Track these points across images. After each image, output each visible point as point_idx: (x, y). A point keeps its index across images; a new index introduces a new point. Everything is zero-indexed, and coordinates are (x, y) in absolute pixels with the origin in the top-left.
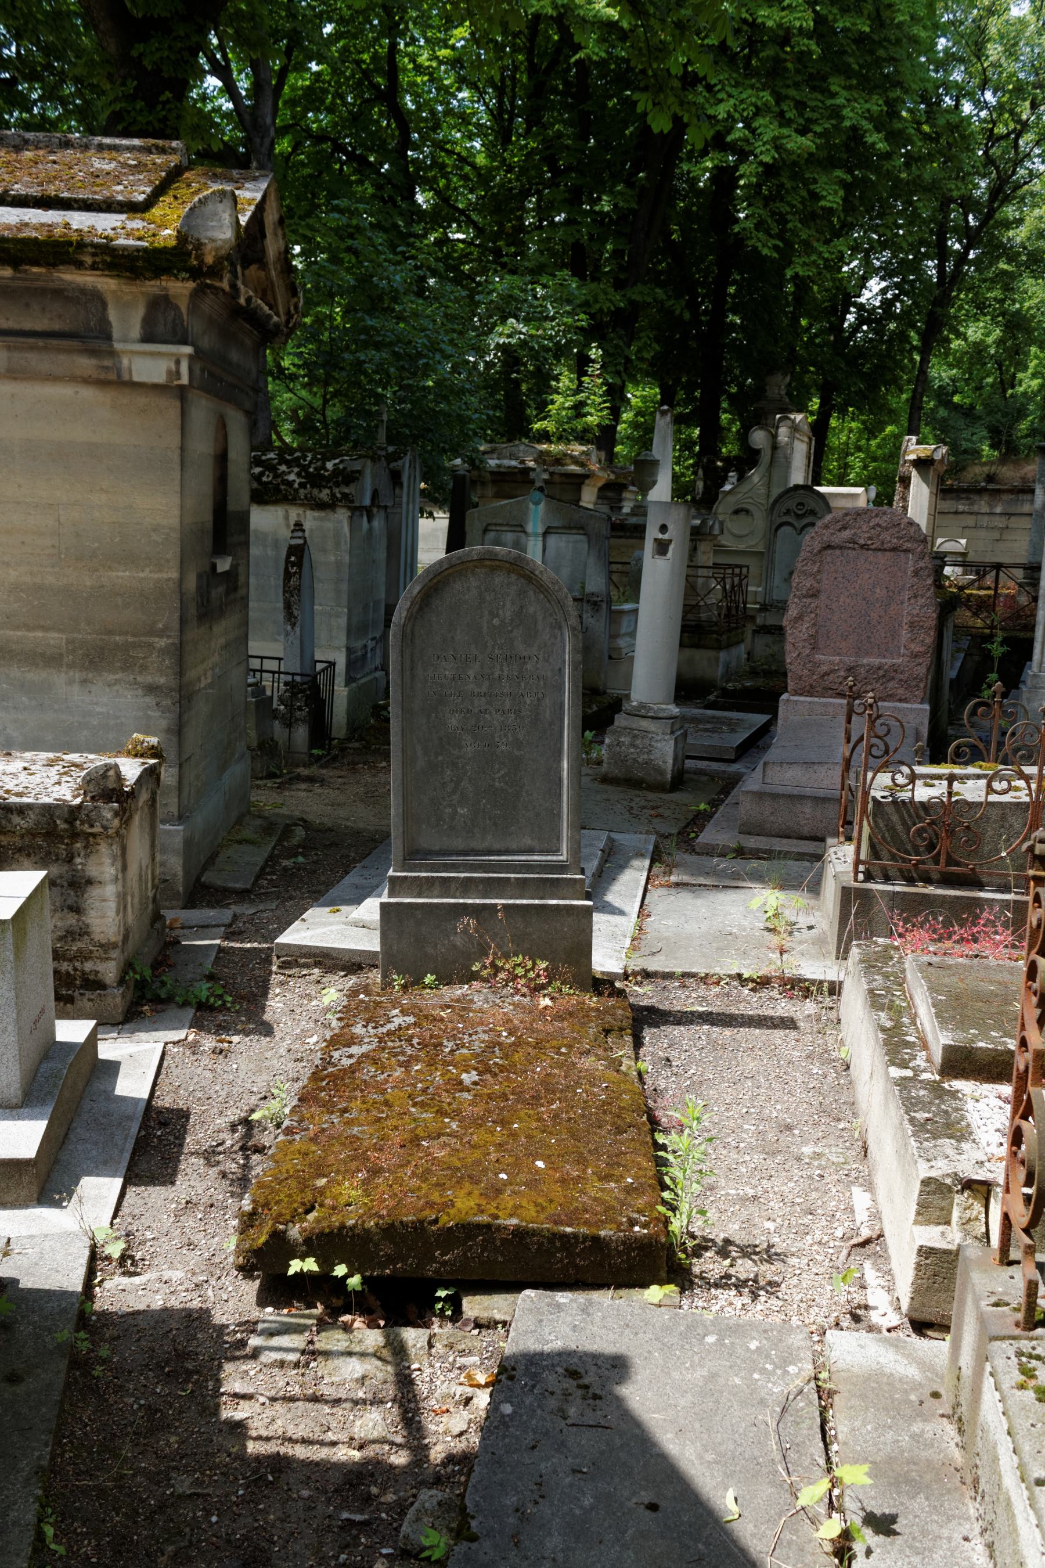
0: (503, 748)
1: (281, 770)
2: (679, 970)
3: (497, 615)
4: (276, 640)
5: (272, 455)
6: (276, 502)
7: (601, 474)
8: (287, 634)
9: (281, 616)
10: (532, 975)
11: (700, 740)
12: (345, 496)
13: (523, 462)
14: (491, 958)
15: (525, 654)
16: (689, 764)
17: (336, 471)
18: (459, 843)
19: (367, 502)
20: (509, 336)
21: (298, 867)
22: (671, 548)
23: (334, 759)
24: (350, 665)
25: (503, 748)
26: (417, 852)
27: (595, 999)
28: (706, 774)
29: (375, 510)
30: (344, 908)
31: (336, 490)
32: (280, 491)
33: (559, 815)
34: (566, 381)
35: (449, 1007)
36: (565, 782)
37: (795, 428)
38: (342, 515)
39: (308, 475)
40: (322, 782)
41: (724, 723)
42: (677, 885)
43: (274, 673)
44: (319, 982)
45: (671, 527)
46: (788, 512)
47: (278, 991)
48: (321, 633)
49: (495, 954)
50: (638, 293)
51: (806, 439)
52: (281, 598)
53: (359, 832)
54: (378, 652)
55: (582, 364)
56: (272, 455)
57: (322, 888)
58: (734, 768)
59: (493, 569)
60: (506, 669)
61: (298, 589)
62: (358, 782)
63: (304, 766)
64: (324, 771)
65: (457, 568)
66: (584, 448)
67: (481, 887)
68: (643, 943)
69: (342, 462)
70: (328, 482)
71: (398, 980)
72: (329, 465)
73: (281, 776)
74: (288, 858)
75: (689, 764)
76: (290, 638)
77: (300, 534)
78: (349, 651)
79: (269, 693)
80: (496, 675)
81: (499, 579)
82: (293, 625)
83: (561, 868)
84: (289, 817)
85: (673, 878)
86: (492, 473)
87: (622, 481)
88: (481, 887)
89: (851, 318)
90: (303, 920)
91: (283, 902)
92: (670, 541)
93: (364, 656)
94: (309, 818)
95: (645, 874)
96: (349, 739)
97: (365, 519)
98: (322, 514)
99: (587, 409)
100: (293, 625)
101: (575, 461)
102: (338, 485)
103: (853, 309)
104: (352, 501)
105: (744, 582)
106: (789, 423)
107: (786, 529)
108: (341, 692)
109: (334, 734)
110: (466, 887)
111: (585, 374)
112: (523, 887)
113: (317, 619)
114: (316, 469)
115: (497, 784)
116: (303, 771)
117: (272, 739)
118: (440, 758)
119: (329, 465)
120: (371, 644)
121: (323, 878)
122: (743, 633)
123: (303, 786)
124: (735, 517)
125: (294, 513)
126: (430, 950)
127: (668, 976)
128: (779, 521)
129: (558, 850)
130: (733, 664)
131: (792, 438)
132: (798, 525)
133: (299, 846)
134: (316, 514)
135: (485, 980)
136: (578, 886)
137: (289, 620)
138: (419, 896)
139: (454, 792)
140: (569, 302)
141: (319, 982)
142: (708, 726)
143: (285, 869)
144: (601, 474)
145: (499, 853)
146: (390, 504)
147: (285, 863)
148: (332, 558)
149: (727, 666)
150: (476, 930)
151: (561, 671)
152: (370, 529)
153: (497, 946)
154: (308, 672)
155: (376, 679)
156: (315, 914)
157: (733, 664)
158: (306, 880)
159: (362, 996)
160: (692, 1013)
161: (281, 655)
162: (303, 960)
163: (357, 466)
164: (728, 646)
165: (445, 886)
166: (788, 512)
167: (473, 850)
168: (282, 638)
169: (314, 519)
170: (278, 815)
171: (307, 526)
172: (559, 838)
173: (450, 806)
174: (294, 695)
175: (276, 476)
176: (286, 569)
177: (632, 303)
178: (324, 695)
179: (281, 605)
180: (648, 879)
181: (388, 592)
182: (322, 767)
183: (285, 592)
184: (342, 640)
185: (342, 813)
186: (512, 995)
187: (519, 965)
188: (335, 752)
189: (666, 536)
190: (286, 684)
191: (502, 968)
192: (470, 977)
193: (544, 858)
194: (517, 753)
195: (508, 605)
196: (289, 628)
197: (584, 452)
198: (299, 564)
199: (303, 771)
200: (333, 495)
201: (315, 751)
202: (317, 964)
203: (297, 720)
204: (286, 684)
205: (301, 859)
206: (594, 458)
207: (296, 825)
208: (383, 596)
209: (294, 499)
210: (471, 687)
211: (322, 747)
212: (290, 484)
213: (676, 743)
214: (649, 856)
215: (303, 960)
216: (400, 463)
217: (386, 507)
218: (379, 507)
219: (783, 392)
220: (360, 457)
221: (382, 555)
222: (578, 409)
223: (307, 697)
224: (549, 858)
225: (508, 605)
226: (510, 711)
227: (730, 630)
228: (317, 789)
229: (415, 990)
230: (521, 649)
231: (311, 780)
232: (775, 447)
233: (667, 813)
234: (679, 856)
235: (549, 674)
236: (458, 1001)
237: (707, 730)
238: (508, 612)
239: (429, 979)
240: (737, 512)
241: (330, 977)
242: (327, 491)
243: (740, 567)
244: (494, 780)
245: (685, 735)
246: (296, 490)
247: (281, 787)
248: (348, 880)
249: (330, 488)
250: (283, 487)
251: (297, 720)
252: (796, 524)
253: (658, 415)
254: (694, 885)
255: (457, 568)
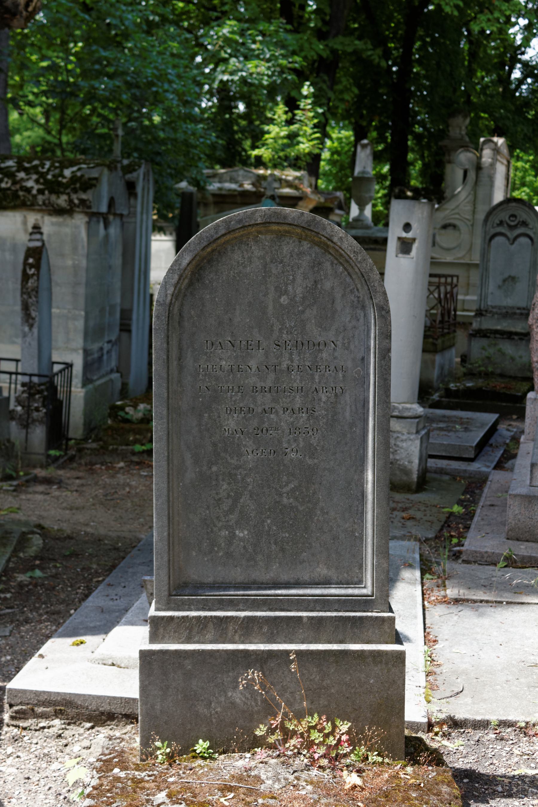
0: (293, 455)
1: (17, 472)
2: (494, 718)
3: (286, 292)
4: (13, 343)
5: (10, 163)
6: (14, 208)
7: (312, 197)
8: (25, 335)
9: (18, 319)
10: (331, 741)
11: (442, 440)
12: (83, 202)
13: (241, 185)
14: (279, 719)
15: (320, 339)
16: (432, 463)
17: (74, 179)
18: (238, 574)
19: (104, 209)
20: (231, 74)
21: (35, 583)
22: (415, 247)
23: (72, 459)
24: (87, 366)
25: (293, 455)
26: (185, 585)
27: (409, 769)
28: (447, 474)
29: (111, 218)
30: (87, 639)
31: (74, 197)
32: (18, 197)
33: (361, 538)
34: (280, 111)
35: (230, 789)
36: (370, 497)
37: (496, 150)
38: (79, 221)
39: (47, 182)
40: (60, 483)
41: (455, 422)
42: (457, 601)
43: (11, 373)
44: (60, 736)
45: (414, 226)
46: (501, 223)
47: (10, 750)
48: (59, 337)
49: (285, 715)
50: (340, 43)
51: (505, 162)
52: (19, 302)
53: (99, 540)
54: (114, 355)
55: (292, 104)
56: (10, 163)
57: (62, 607)
58: (475, 467)
59: (280, 236)
60: (295, 357)
61: (36, 290)
62: (96, 484)
63: (42, 467)
64: (61, 472)
65: (237, 234)
66: (298, 174)
67: (265, 629)
68: (440, 679)
69: (79, 169)
70: (67, 188)
71: (162, 749)
72: (67, 173)
73: (17, 478)
74: (24, 571)
75: (432, 463)
76: (28, 339)
77: (38, 236)
78: (86, 352)
79: (5, 394)
80: (284, 366)
81: (288, 247)
82: (31, 326)
83: (365, 603)
84: (26, 524)
85: (451, 592)
86: (214, 195)
87: (329, 205)
88: (265, 629)
89: (517, 74)
90: (41, 656)
91: (18, 626)
92: (414, 240)
93: (100, 358)
94: (47, 523)
95: (419, 588)
96: (85, 439)
97: (102, 225)
98: (59, 219)
99: (300, 139)
100: (31, 326)
101: (289, 184)
102: (75, 191)
103: (519, 66)
104: (89, 207)
105: (455, 290)
106: (492, 145)
107: (499, 239)
108: (78, 392)
109: (71, 435)
110: (247, 629)
111: (298, 107)
112: (317, 629)
113: (54, 322)
114: (54, 176)
115: (285, 501)
116: (40, 472)
117: (9, 441)
118: (214, 469)
119: (67, 173)
120: (106, 347)
121: (62, 596)
122: (454, 338)
123: (41, 488)
124: (443, 231)
125: (32, 218)
126: (202, 710)
127: (483, 725)
128: (493, 231)
129: (360, 582)
130: (447, 367)
131: (495, 160)
132: (512, 234)
133: (36, 558)
134: (54, 219)
135: (272, 747)
136: (386, 627)
137: (27, 321)
138: (188, 641)
139: (231, 510)
140: (283, 47)
141: (60, 736)
142: (442, 425)
143: (21, 586)
144: (312, 197)
145: (287, 585)
146: (125, 212)
147: (22, 578)
148: (70, 263)
149: (442, 368)
150: (263, 686)
151: (364, 360)
152: (107, 236)
153: (289, 704)
154: (46, 372)
155: (111, 380)
156: (56, 648)
157: (447, 367)
158: (43, 598)
159: (116, 770)
160: (522, 778)
161: (18, 357)
162: (40, 710)
163: (94, 174)
164: (444, 349)
165: (221, 629)
166: (501, 223)
167: (254, 582)
168: (19, 340)
169: (53, 224)
170: (13, 521)
171: (46, 229)
172: (361, 566)
173: (227, 527)
174: (31, 395)
175: (14, 183)
176: (24, 272)
177: (334, 52)
178: (61, 396)
179: (18, 308)
180: (423, 594)
181: (123, 297)
182: (59, 468)
183: (22, 293)
184: (79, 342)
185: (81, 517)
186: (307, 768)
187: (314, 727)
188: (72, 452)
189: (410, 235)
190: (23, 385)
191: (294, 732)
192: (253, 744)
193: (343, 592)
194: (310, 462)
195: (299, 279)
196: (27, 329)
197: (297, 178)
198: (37, 266)
199: (40, 472)
200: (71, 201)
201: (52, 452)
202: (58, 714)
203: (34, 421)
204: (23, 385)
205: (38, 573)
206: (306, 182)
207: (33, 533)
208: (118, 300)
209: (32, 205)
210: (253, 380)
211: (59, 448)
212: (28, 190)
213: (421, 442)
214: (417, 565)
215: (40, 710)
216: (135, 174)
217: (121, 216)
218: (115, 215)
219: (464, 133)
220: (98, 165)
221: (117, 261)
222: (292, 137)
223: (45, 398)
224: (350, 591)
225: (299, 279)
226: (300, 410)
227: (443, 335)
228: (54, 490)
229: (184, 762)
230: (314, 333)
231: (48, 481)
232: (479, 167)
233: (418, 515)
234: (448, 565)
235: (349, 364)
236: (240, 779)
237: (441, 429)
238: (298, 290)
239: (201, 746)
240: (445, 227)
241: (73, 730)
242: (64, 197)
243: (452, 276)
244: (281, 495)
245: (428, 434)
246: (35, 196)
247: (17, 490)
248: (93, 601)
249: (68, 194)
250: (21, 193)
251: (34, 421)
252: (509, 234)
253: (359, 148)
254: (475, 601)
255: (237, 234)
